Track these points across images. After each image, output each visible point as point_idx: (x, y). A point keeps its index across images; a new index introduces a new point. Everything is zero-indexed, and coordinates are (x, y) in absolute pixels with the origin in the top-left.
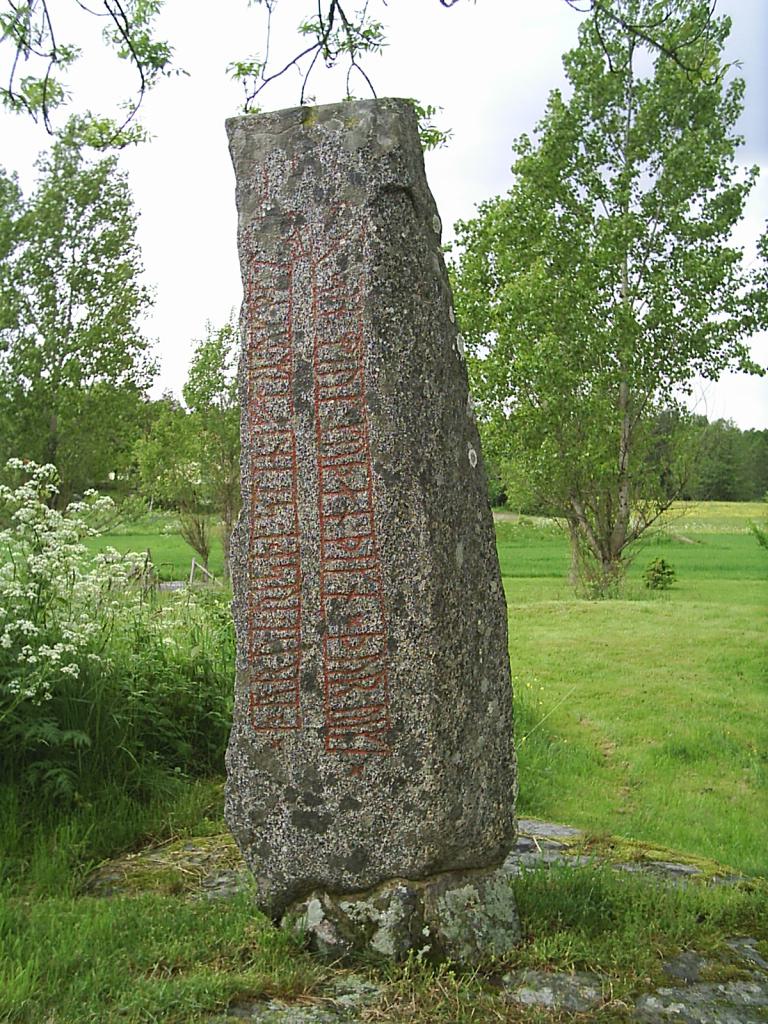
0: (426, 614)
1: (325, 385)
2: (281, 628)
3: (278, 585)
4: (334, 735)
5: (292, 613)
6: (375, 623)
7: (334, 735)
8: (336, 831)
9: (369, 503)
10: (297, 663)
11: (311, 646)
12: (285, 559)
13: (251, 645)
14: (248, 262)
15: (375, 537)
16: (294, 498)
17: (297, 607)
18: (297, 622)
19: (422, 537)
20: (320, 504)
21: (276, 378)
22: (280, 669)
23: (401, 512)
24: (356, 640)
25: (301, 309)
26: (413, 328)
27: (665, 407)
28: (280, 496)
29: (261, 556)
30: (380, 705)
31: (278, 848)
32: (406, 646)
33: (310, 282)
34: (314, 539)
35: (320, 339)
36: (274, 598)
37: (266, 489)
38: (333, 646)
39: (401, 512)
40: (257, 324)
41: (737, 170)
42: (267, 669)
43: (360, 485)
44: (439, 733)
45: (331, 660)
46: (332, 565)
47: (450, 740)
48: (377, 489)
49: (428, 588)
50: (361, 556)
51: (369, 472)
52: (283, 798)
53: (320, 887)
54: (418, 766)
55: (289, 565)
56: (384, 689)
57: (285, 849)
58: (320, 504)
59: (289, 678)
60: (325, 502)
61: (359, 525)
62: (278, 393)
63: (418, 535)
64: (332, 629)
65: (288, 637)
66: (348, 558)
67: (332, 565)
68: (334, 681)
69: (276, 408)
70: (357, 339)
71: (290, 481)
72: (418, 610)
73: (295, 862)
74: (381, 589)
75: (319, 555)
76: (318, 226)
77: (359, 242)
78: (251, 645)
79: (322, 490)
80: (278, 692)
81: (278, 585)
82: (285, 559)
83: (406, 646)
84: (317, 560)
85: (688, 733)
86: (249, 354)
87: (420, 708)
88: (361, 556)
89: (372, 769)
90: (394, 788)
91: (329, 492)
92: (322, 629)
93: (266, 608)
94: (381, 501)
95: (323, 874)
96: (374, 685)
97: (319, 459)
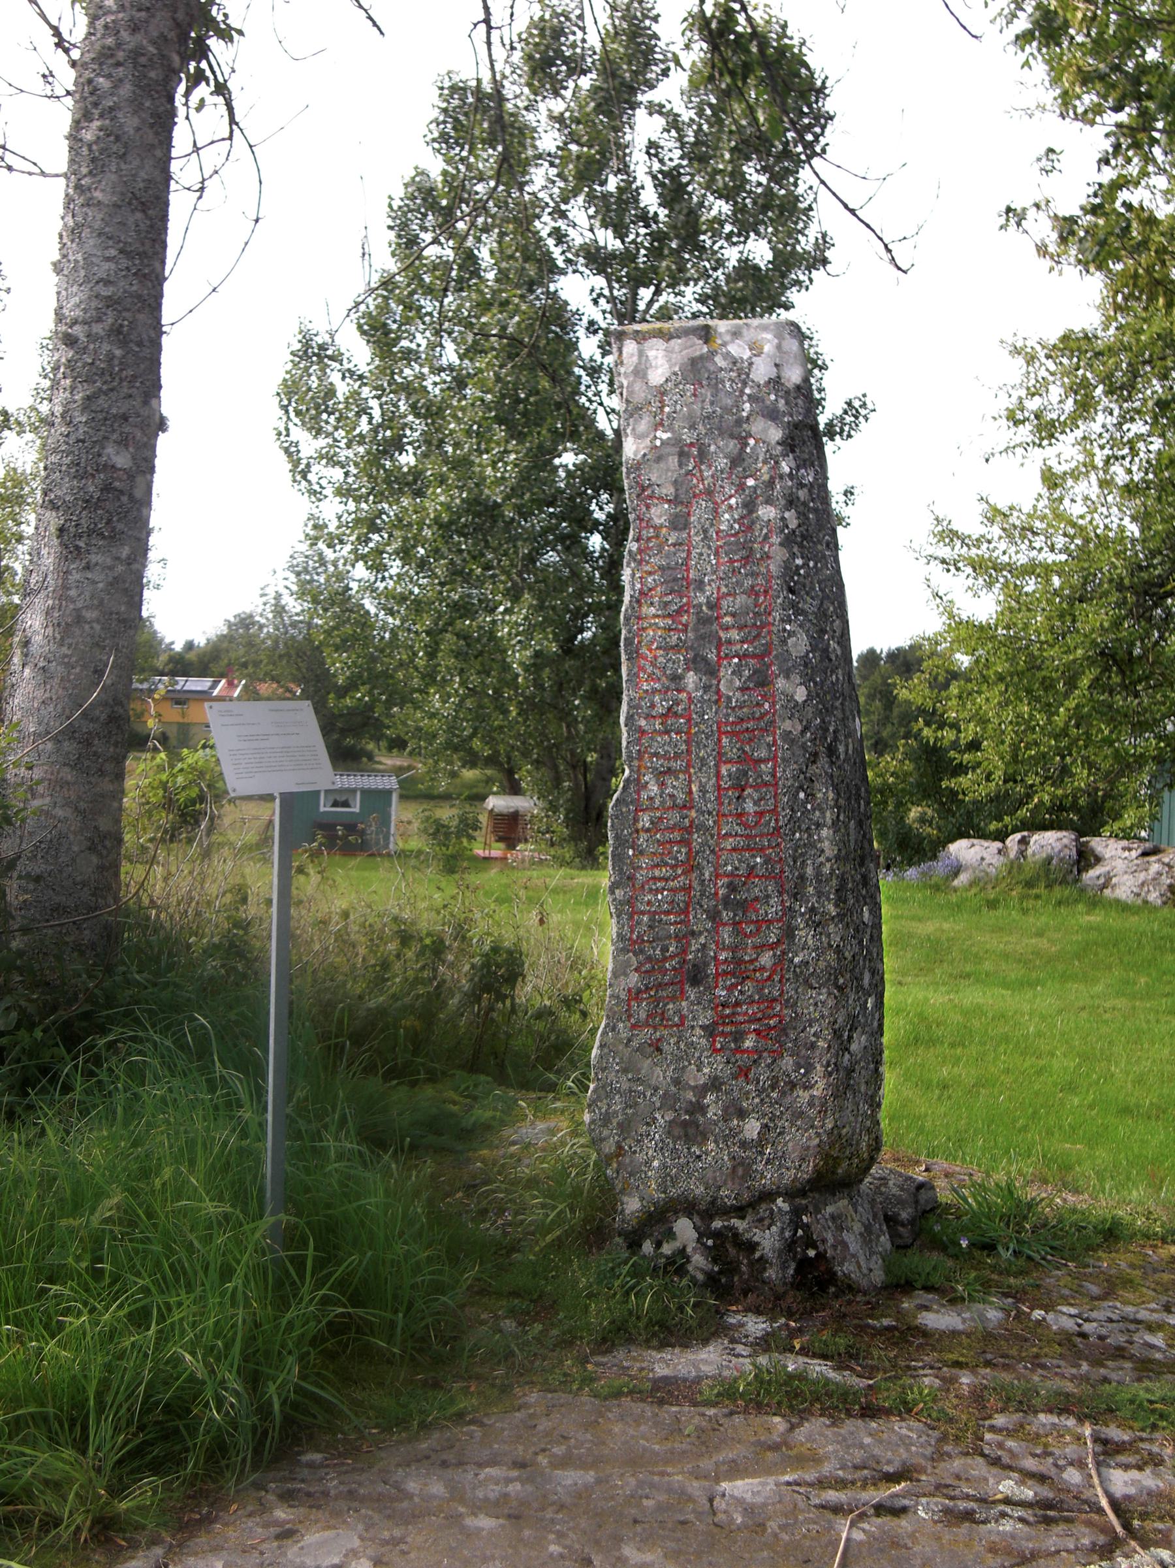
0: (829, 899)
1: (729, 642)
2: (668, 913)
3: (666, 864)
4: (723, 1034)
5: (680, 897)
6: (773, 909)
7: (723, 1034)
8: (716, 1142)
9: (774, 775)
10: (684, 952)
11: (701, 933)
12: (676, 836)
13: (632, 932)
14: (638, 496)
15: (778, 814)
16: (689, 765)
17: (688, 889)
18: (687, 904)
19: (828, 814)
20: (718, 775)
21: (670, 630)
22: (665, 959)
23: (807, 783)
24: (752, 927)
25: (701, 554)
26: (819, 582)
27: (459, 214)
28: (673, 764)
29: (648, 830)
30: (774, 1000)
31: (648, 1163)
32: (805, 935)
33: (712, 525)
34: (710, 813)
35: (724, 590)
36: (660, 879)
37: (656, 754)
38: (726, 935)
39: (807, 783)
40: (648, 568)
41: (1002, 221)
42: (649, 959)
43: (763, 754)
44: (835, 1032)
45: (723, 949)
46: (729, 843)
47: (841, 1041)
48: (783, 759)
49: (832, 870)
50: (761, 836)
51: (775, 741)
52: (658, 1105)
53: (689, 1207)
54: (810, 1068)
55: (679, 842)
56: (780, 981)
57: (656, 1163)
58: (718, 775)
59: (674, 969)
60: (724, 772)
61: (760, 800)
62: (672, 648)
63: (823, 813)
64: (726, 915)
65: (676, 923)
66: (748, 836)
67: (729, 843)
68: (725, 973)
69: (670, 665)
70: (766, 592)
71: (684, 747)
72: (819, 894)
73: (666, 1180)
74: (782, 872)
75: (715, 831)
76: (722, 462)
77: (771, 484)
78: (632, 932)
79: (720, 758)
80: (660, 985)
81: (666, 864)
82: (676, 836)
83: (805, 935)
84: (712, 836)
85: (217, 821)
86: (638, 601)
87: (816, 1004)
88: (761, 836)
89: (763, 1074)
90: (783, 1094)
91: (729, 761)
92: (714, 916)
93: (651, 890)
94: (786, 774)
95: (697, 1192)
96: (769, 978)
97: (719, 724)
